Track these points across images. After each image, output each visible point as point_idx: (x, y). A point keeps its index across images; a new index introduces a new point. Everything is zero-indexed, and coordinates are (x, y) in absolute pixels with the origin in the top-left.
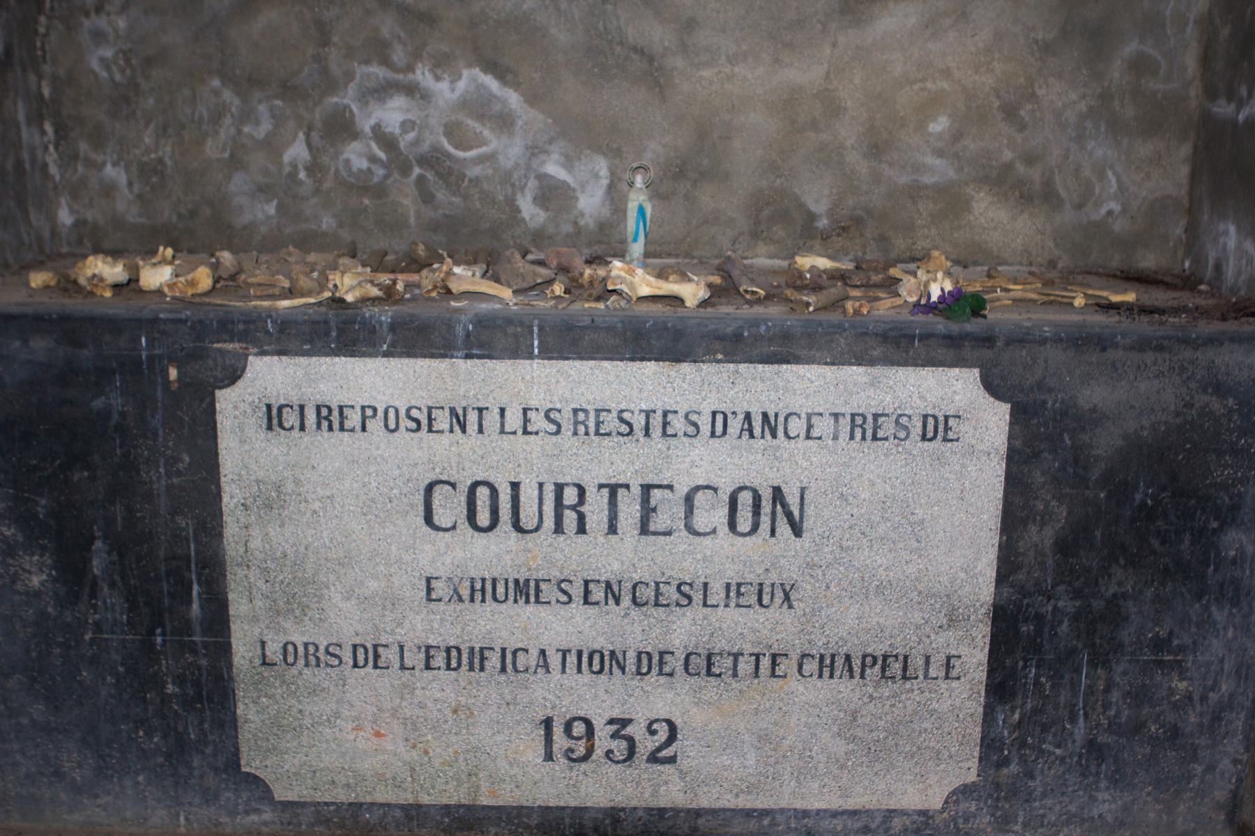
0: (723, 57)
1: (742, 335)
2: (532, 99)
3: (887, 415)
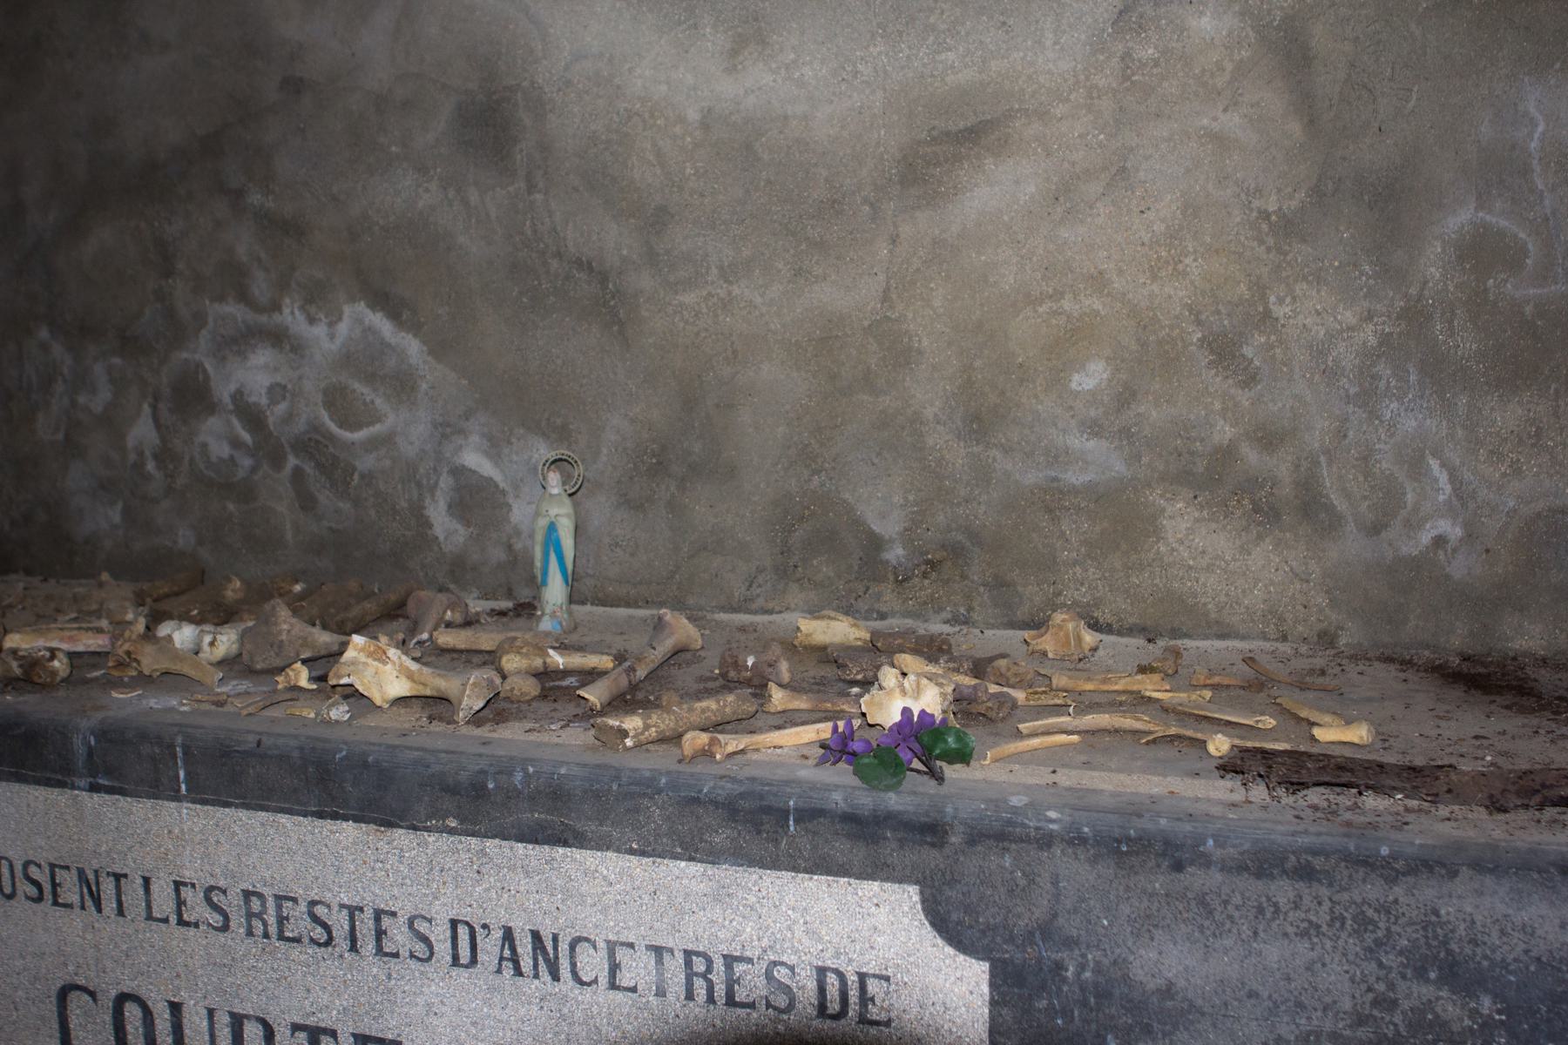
0: (714, 271)
1: (484, 787)
2: (439, 349)
3: (750, 961)
